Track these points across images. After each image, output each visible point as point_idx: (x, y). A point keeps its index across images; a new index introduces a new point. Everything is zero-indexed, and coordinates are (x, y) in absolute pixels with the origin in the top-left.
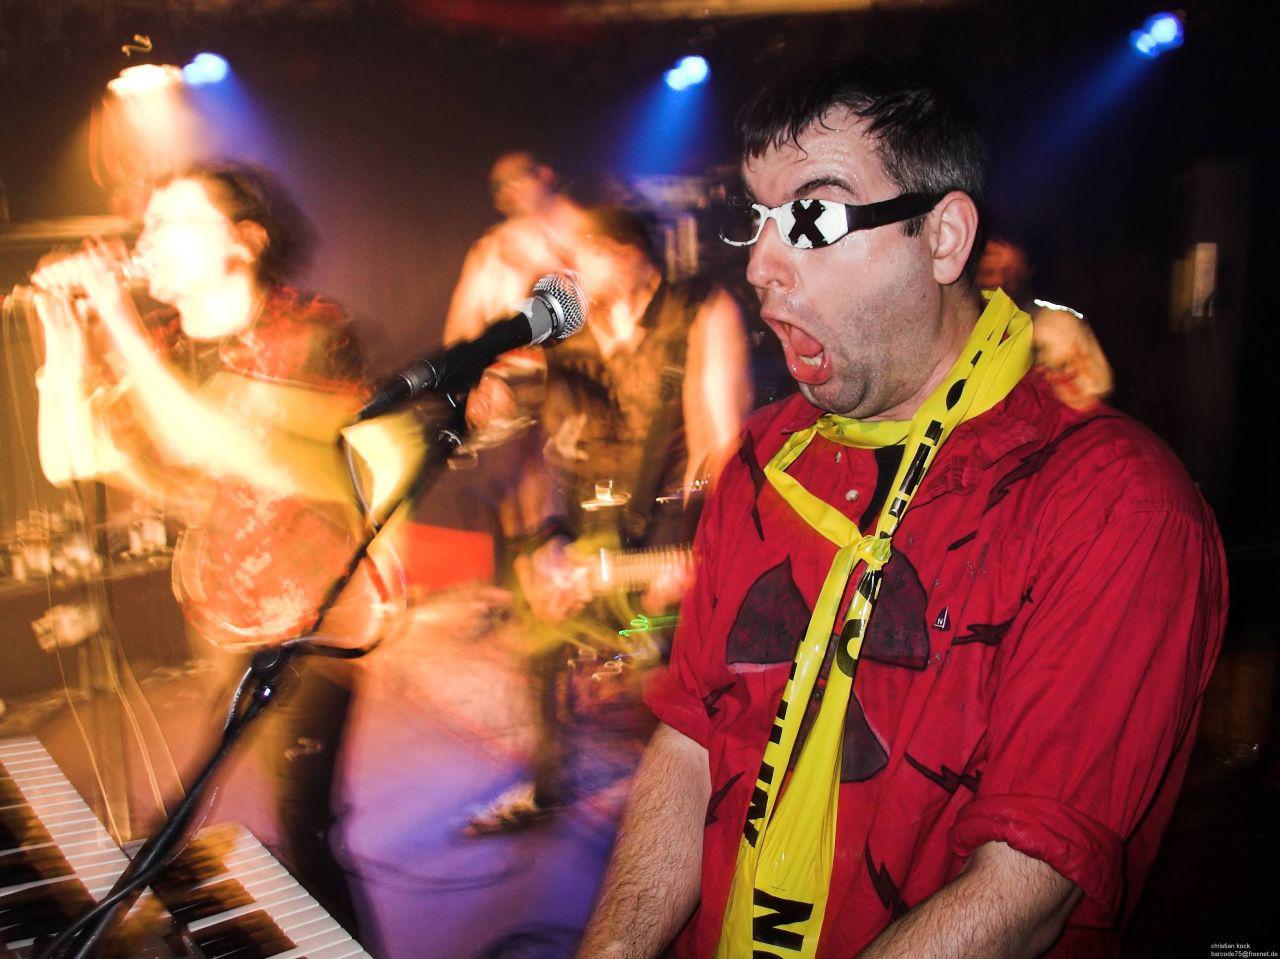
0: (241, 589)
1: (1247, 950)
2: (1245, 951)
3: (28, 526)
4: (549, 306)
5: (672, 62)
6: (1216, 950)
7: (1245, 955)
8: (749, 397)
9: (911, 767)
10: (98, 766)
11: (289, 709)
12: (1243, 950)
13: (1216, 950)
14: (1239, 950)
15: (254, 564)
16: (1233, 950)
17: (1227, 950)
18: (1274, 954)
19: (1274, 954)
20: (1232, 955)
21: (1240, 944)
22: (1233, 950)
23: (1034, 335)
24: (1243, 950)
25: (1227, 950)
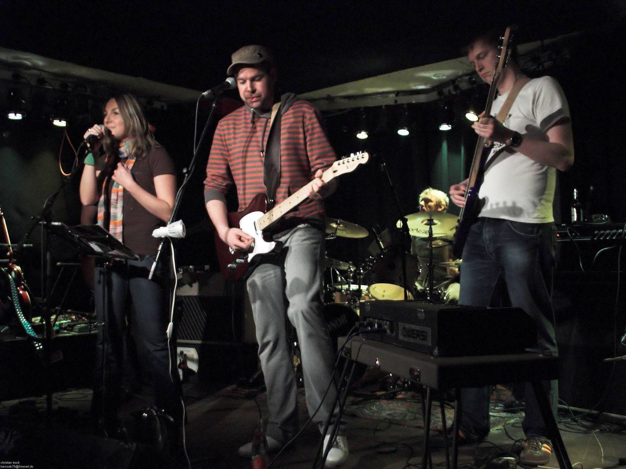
0: (117, 189)
1: (18, 465)
2: (17, 465)
3: (253, 80)
4: (256, 79)
5: (402, 128)
6: (3, 465)
7: (17, 467)
8: (226, 211)
9: (571, 457)
10: (562, 460)
11: (52, 320)
12: (16, 465)
13: (3, 465)
14: (14, 464)
15: (106, 144)
16: (11, 465)
17: (8, 465)
18: (32, 467)
19: (32, 467)
20: (10, 467)
21: (15, 461)
22: (11, 465)
23: (283, 268)
24: (16, 465)
25: (8, 465)
